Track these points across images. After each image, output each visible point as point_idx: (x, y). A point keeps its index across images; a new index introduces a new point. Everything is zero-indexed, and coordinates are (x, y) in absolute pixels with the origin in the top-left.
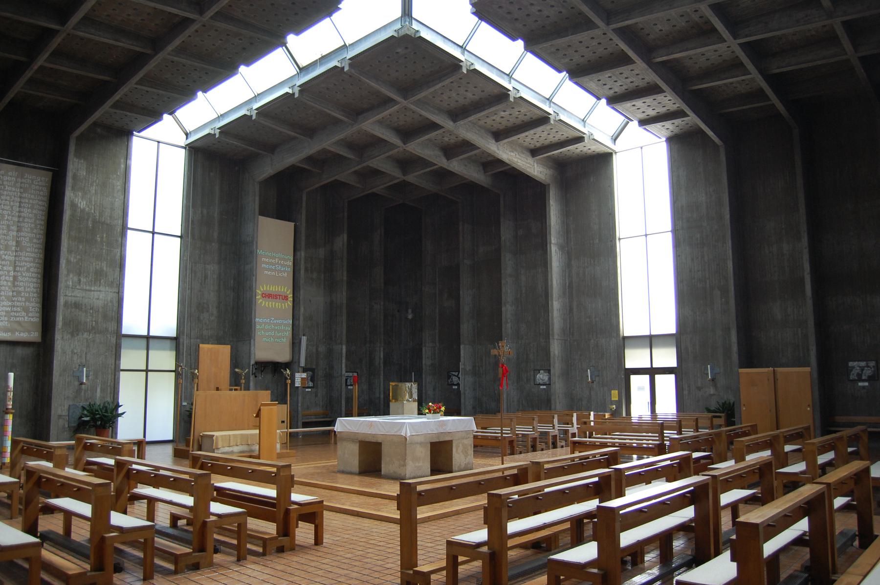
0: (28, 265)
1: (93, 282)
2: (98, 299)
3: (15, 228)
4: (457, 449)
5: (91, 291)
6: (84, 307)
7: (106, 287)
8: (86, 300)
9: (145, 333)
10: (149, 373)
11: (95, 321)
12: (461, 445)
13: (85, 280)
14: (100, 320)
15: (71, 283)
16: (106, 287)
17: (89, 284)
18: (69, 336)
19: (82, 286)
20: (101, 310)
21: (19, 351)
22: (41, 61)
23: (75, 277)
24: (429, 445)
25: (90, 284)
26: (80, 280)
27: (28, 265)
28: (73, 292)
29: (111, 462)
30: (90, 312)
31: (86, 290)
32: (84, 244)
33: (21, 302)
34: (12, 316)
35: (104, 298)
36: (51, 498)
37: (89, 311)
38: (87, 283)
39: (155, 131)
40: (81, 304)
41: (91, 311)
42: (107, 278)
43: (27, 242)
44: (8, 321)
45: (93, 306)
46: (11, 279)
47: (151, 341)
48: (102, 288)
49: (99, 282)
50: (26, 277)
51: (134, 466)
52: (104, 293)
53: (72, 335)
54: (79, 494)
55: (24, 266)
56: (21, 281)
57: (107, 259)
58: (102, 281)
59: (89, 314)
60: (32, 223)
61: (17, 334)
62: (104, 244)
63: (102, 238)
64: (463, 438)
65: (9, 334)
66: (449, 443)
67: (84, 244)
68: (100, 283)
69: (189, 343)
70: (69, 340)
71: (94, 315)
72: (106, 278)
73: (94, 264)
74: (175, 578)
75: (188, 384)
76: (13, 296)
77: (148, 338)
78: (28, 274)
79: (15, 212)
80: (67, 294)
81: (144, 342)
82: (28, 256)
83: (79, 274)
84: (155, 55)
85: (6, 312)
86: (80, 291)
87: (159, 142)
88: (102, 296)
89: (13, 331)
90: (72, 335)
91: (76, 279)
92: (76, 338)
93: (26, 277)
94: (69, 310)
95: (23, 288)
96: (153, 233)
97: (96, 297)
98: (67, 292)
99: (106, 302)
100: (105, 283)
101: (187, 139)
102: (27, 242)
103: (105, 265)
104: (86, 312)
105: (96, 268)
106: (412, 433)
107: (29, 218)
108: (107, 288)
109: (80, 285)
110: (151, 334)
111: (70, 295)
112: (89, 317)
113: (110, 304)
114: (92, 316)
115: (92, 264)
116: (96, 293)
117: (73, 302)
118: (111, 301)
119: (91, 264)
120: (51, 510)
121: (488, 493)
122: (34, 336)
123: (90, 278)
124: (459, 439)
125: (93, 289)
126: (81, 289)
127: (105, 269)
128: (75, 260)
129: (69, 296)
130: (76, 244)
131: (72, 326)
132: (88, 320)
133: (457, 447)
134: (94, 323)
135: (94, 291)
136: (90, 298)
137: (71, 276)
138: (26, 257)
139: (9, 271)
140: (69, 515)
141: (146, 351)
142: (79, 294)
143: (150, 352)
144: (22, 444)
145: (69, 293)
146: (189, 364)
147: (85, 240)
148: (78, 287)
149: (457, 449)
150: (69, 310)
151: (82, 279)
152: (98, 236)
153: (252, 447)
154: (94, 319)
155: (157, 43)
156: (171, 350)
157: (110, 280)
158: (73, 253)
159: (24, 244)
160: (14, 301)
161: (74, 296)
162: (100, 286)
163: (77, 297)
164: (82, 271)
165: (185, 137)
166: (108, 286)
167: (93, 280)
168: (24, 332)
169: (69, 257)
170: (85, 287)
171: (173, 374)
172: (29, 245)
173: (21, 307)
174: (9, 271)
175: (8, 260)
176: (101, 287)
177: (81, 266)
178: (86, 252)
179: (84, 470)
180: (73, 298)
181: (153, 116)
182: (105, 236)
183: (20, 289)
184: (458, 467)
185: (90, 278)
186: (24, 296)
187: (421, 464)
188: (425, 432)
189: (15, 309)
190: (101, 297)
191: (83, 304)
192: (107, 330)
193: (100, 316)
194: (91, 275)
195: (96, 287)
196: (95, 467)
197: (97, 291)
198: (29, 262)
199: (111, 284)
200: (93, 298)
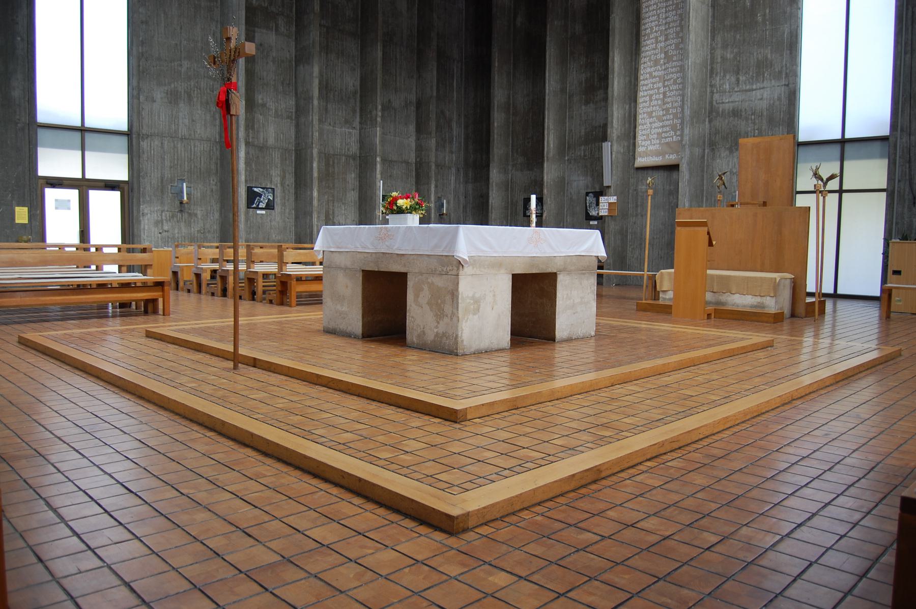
0: (675, 76)
1: (755, 78)
2: (761, 99)
3: (662, 38)
4: (417, 296)
5: (753, 90)
6: (743, 114)
7: (771, 80)
8: (747, 104)
10: (844, 195)
11: (758, 129)
12: (426, 287)
13: (744, 78)
14: (763, 127)
15: (728, 86)
16: (771, 80)
17: (749, 82)
18: (727, 152)
19: (741, 86)
20: (765, 113)
23: (732, 77)
24: (360, 276)
25: (751, 80)
26: (738, 80)
27: (675, 76)
28: (731, 96)
30: (751, 118)
31: (746, 91)
32: (742, 31)
33: (669, 120)
34: (662, 138)
35: (769, 97)
37: (750, 117)
38: (747, 82)
40: (741, 110)
41: (753, 117)
42: (772, 69)
43: (673, 50)
44: (659, 143)
45: (755, 110)
46: (661, 96)
48: (766, 84)
49: (761, 76)
50: (672, 90)
52: (768, 89)
53: (731, 152)
55: (671, 78)
56: (668, 97)
57: (772, 42)
58: (766, 75)
59: (750, 122)
60: (676, 27)
61: (667, 156)
62: (767, 23)
63: (764, 15)
64: (433, 273)
65: (661, 158)
66: (400, 279)
67: (742, 31)
68: (764, 77)
69: (906, 142)
70: (726, 158)
71: (757, 121)
72: (771, 67)
73: (755, 54)
74: (193, 357)
75: (906, 210)
76: (663, 115)
78: (675, 87)
79: (661, 20)
80: (724, 101)
81: (836, 149)
82: (674, 67)
83: (737, 73)
85: (658, 134)
86: (739, 93)
88: (766, 94)
89: (662, 154)
90: (731, 152)
91: (733, 79)
92: (735, 154)
93: (672, 90)
94: (727, 121)
95: (670, 104)
97: (759, 97)
98: (724, 98)
99: (772, 102)
100: (770, 75)
102: (673, 50)
103: (769, 52)
104: (747, 119)
105: (757, 59)
106: (331, 247)
107: (674, 21)
108: (773, 81)
109: (738, 86)
111: (727, 101)
112: (750, 125)
113: (777, 103)
114: (754, 123)
115: (753, 54)
116: (758, 93)
117: (731, 109)
118: (779, 99)
119: (752, 56)
123: (751, 73)
124: (421, 274)
125: (754, 87)
126: (739, 91)
127: (769, 56)
128: (732, 56)
129: (726, 103)
130: (732, 34)
131: (730, 140)
132: (749, 129)
133: (418, 291)
134: (757, 131)
135: (755, 90)
136: (752, 101)
137: (728, 77)
138: (672, 68)
139: (658, 88)
141: (80, 152)
142: (737, 97)
143: (846, 163)
145: (726, 99)
146: (907, 177)
147: (742, 26)
148: (736, 89)
149: (417, 296)
150: (727, 121)
151: (741, 78)
152: (759, 15)
153: (721, 298)
154: (756, 127)
156: (882, 157)
157: (777, 70)
158: (729, 47)
159: (671, 53)
160: (663, 121)
161: (732, 102)
162: (763, 81)
163: (735, 102)
164: (741, 68)
166: (774, 79)
167: (754, 75)
168: (673, 154)
169: (725, 53)
170: (744, 88)
171: (884, 194)
172: (675, 53)
173: (669, 125)
174: (658, 88)
175: (657, 76)
176: (765, 82)
177: (739, 61)
178: (744, 40)
180: (731, 104)
182: (767, 11)
183: (668, 106)
184: (419, 336)
185: (751, 73)
186: (672, 113)
187: (345, 309)
188: (351, 248)
189: (665, 130)
190: (765, 96)
191: (743, 110)
193: (764, 121)
194: (751, 69)
195: (758, 84)
197: (760, 89)
198: (675, 73)
199: (778, 76)
200: (755, 99)
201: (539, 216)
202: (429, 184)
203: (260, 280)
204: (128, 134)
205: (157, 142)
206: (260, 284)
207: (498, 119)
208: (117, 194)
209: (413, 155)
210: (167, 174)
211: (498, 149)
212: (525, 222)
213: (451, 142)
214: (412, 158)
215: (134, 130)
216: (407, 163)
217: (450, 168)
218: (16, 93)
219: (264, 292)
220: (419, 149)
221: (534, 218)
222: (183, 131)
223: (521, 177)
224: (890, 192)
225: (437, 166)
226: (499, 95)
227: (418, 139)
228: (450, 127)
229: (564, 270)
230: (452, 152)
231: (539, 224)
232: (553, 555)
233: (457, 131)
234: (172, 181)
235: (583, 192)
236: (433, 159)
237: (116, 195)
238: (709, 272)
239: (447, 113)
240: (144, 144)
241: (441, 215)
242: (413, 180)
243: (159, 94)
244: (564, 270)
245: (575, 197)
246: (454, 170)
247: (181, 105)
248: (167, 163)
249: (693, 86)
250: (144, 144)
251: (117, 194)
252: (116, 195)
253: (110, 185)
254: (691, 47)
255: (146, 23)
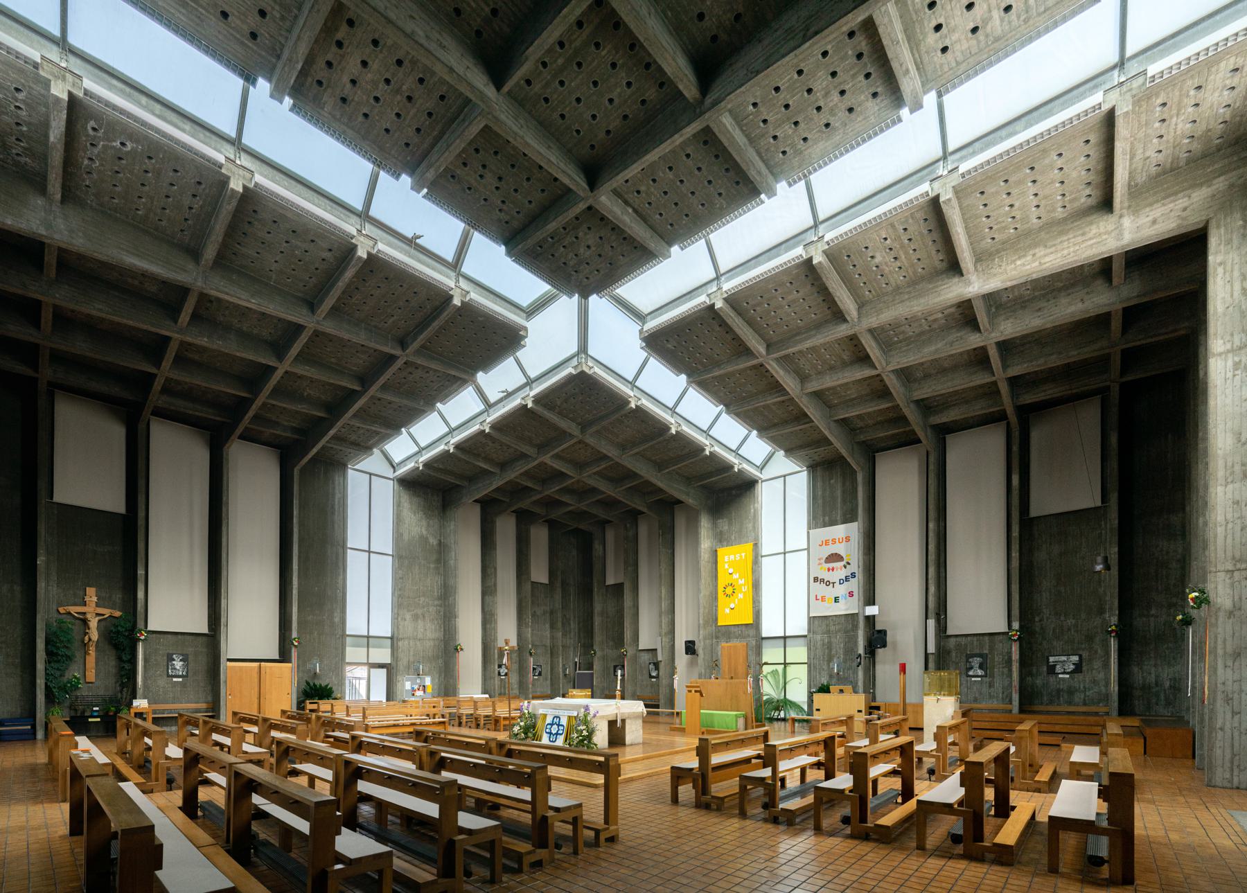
9: (783, 635)
21: (200, 639)
22: (373, 390)
29: (347, 736)
36: (295, 764)
39: (372, 462)
47: (788, 641)
51: (364, 739)
54: (322, 760)
77: (785, 638)
81: (782, 640)
84: (366, 391)
87: (371, 474)
96: (369, 552)
101: (394, 472)
110: (787, 635)
120: (295, 773)
121: (846, 747)
122: (204, 629)
140: (312, 779)
141: (783, 649)
143: (370, 649)
144: (211, 724)
155: (365, 380)
165: (392, 470)
179: (323, 742)
181: (364, 447)
192: (749, 636)
196: (332, 740)
201: (623, 691)
202: (558, 658)
203: (464, 717)
204: (392, 638)
205: (406, 642)
206: (464, 719)
207: (597, 621)
208: (385, 670)
209: (548, 641)
210: (411, 659)
211: (598, 637)
212: (614, 697)
213: (570, 632)
214: (548, 643)
215: (395, 635)
216: (545, 646)
217: (569, 647)
218: (337, 620)
219: (484, 724)
220: (552, 638)
221: (618, 693)
222: (420, 636)
223: (612, 653)
224: (809, 664)
225: (563, 646)
226: (598, 607)
227: (551, 632)
228: (570, 624)
229: (629, 718)
230: (570, 638)
231: (623, 698)
232: (640, 874)
233: (574, 625)
234: (414, 662)
235: (648, 662)
236: (560, 644)
237: (384, 671)
238: (702, 711)
239: (568, 616)
240: (400, 644)
241: (565, 675)
242: (549, 655)
243: (408, 616)
244: (629, 718)
245: (643, 665)
246: (572, 649)
247: (420, 621)
248: (412, 653)
249: (704, 607)
250: (400, 644)
251: (385, 670)
252: (384, 671)
253: (381, 666)
254: (702, 587)
255: (402, 578)
